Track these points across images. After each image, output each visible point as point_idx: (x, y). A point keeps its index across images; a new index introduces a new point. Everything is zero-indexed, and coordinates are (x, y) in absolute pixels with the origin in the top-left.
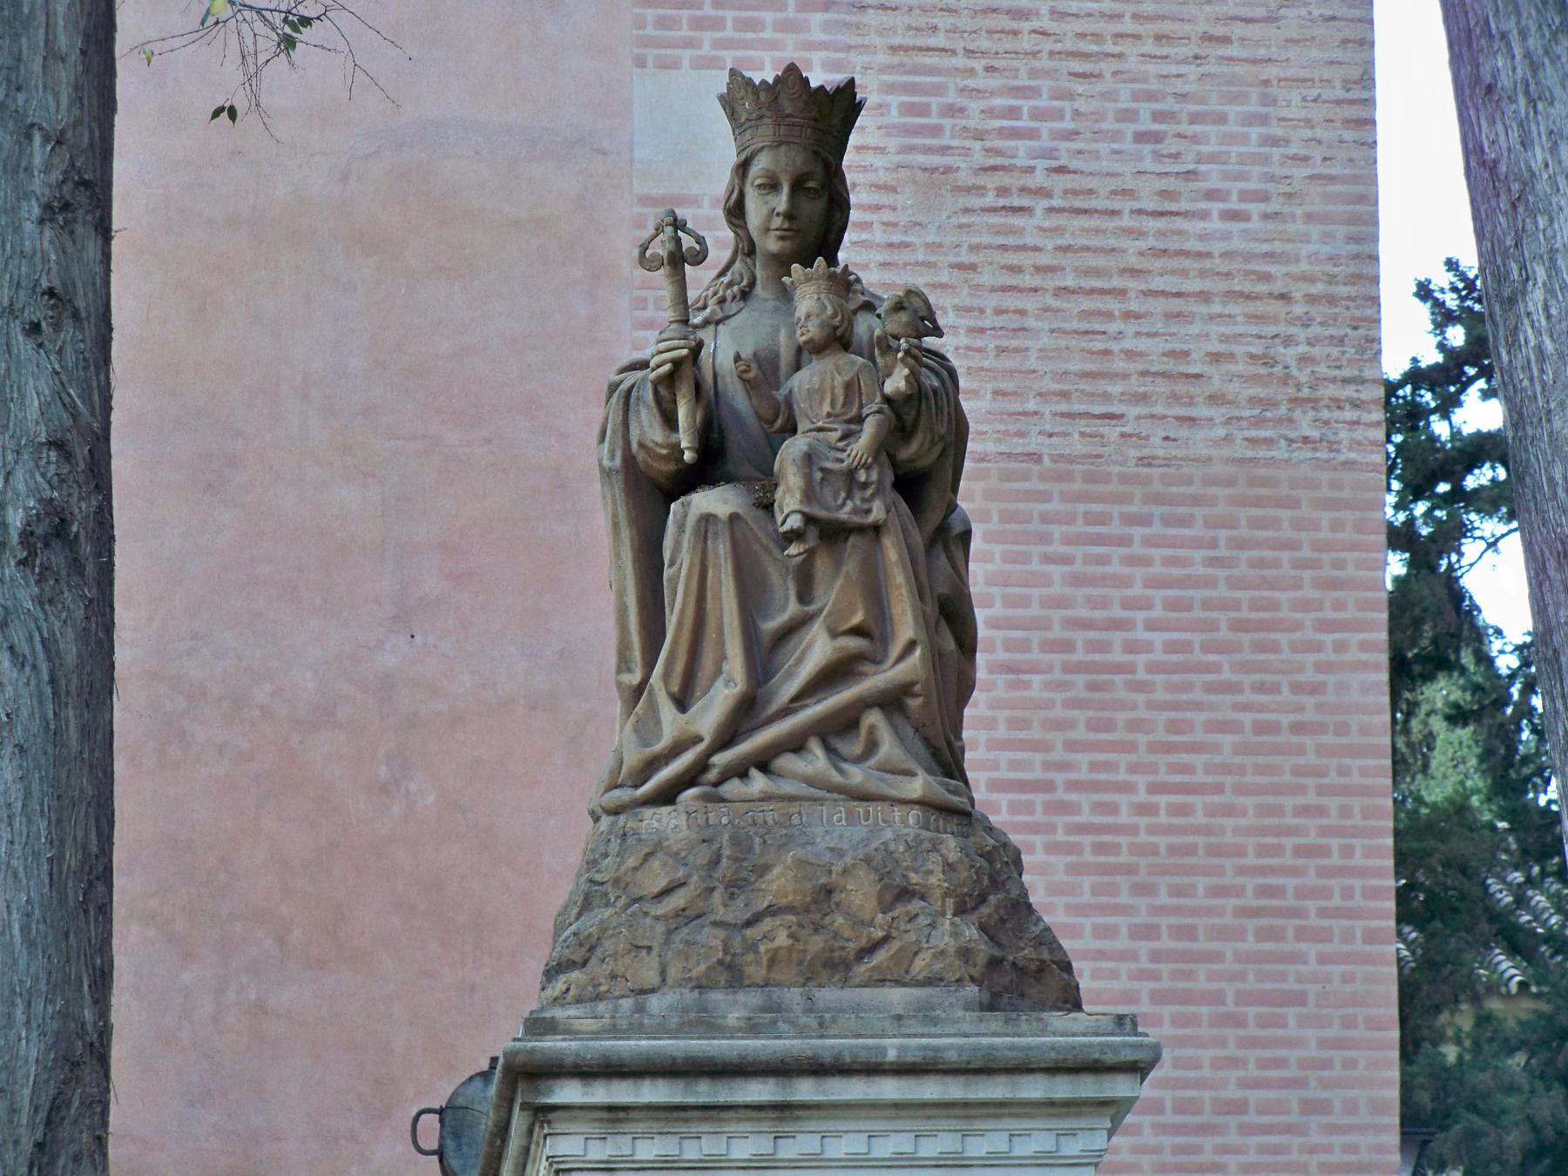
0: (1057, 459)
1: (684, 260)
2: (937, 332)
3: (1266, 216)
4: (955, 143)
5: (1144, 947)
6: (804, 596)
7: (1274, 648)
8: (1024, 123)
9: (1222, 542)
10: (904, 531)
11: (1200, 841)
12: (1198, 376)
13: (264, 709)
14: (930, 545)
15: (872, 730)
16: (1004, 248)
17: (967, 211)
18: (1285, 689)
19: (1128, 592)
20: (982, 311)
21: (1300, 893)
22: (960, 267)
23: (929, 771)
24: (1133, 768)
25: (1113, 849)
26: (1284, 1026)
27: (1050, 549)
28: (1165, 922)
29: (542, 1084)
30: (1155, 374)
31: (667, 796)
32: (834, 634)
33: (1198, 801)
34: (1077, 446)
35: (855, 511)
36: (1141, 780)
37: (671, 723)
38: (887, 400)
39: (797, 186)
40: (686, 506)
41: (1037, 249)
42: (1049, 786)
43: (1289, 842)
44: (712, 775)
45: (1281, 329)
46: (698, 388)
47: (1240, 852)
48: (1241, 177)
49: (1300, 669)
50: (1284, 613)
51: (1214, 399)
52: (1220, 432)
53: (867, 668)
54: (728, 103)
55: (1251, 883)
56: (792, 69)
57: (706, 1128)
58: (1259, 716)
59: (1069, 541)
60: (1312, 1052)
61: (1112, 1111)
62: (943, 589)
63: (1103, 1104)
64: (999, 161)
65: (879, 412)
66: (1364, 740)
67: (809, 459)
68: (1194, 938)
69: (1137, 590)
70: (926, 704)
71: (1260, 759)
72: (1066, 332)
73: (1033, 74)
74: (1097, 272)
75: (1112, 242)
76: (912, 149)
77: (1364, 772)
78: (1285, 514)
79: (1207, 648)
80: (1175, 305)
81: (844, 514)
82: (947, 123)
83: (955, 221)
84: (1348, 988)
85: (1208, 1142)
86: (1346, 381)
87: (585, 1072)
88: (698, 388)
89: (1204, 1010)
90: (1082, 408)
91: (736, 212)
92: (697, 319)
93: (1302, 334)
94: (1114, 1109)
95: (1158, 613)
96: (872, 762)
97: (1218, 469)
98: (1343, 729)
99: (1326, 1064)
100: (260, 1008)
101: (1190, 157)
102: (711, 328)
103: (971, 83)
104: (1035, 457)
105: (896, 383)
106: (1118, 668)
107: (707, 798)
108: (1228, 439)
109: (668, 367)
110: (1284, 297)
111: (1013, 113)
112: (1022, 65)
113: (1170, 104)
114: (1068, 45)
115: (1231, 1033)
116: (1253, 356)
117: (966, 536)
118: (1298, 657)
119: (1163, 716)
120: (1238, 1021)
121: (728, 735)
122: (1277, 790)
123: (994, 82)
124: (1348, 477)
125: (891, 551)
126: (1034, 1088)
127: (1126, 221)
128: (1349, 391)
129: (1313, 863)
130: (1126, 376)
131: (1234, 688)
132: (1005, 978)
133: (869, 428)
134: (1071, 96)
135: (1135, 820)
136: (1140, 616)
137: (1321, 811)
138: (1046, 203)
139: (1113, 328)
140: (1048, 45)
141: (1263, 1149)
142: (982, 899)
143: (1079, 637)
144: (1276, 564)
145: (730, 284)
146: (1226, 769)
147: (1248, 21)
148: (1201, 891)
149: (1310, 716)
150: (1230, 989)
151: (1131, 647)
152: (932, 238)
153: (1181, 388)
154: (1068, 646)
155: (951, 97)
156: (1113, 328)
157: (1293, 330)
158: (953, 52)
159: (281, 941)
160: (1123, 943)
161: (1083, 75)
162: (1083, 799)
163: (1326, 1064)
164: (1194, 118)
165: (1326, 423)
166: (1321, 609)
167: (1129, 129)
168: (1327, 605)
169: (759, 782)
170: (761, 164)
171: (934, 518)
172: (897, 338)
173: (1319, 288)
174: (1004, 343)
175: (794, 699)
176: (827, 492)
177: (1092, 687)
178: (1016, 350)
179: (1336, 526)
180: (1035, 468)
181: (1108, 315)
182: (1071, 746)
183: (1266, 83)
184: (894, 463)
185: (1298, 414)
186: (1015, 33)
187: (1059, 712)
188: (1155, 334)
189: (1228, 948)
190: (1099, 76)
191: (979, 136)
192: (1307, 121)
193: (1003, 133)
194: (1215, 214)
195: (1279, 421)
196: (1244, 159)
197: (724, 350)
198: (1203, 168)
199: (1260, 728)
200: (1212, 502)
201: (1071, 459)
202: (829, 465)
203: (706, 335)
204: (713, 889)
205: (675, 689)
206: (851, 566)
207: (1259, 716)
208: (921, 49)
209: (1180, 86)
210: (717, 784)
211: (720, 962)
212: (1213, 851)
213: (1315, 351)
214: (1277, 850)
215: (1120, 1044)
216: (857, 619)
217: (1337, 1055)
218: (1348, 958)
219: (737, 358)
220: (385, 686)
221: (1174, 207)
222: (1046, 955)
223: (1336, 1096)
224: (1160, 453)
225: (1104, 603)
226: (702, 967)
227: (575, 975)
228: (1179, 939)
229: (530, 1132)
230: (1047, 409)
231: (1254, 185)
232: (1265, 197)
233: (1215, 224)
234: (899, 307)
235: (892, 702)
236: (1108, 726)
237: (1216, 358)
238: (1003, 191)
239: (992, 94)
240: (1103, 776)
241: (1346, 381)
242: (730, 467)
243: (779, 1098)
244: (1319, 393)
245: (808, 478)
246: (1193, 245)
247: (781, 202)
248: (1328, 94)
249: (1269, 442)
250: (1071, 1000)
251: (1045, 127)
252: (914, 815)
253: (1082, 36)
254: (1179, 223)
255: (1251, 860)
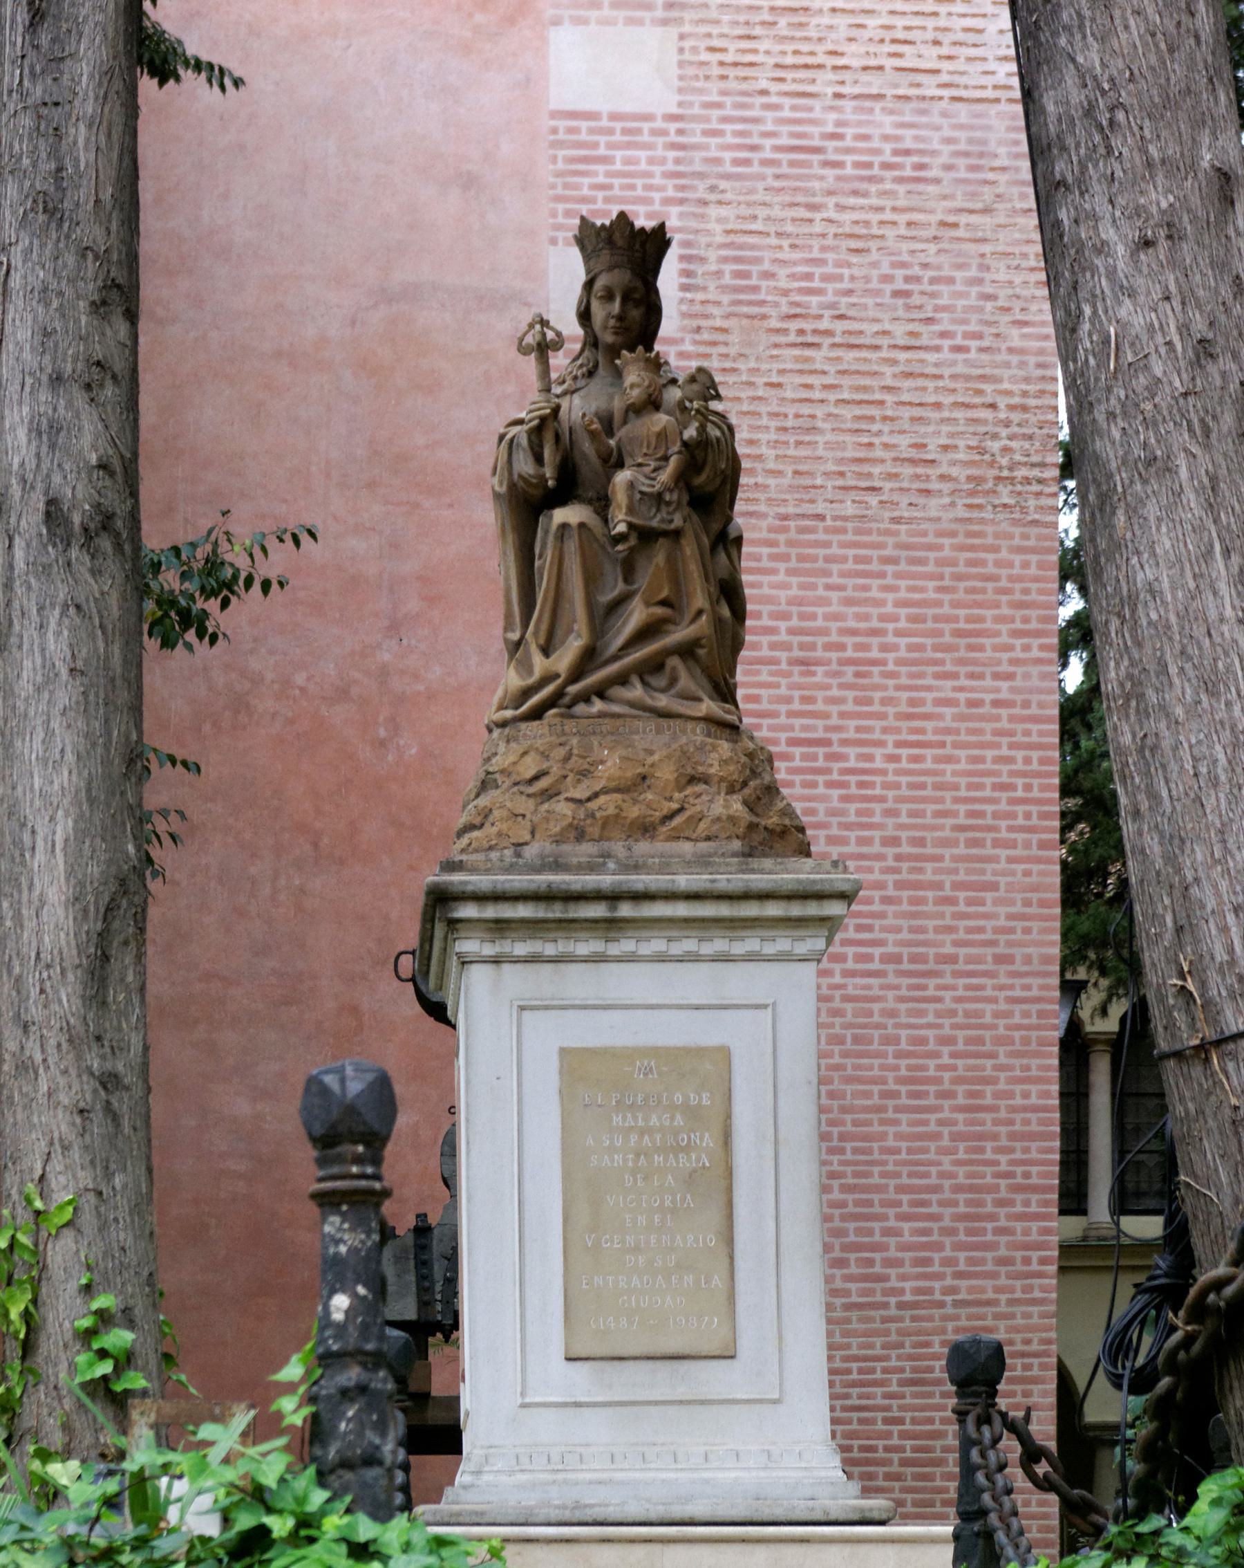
0: (835, 518)
1: (548, 347)
2: (718, 397)
3: (981, 350)
4: (769, 298)
5: (890, 851)
6: (627, 580)
7: (981, 648)
8: (816, 284)
9: (947, 576)
10: (697, 537)
11: (929, 780)
12: (933, 461)
13: (302, 689)
14: (713, 549)
15: (674, 669)
16: (801, 372)
17: (776, 346)
18: (988, 676)
19: (883, 610)
20: (786, 416)
21: (996, 815)
22: (772, 385)
23: (712, 698)
24: (885, 730)
25: (871, 785)
26: (984, 904)
27: (830, 581)
28: (904, 835)
29: (453, 904)
30: (904, 460)
31: (536, 714)
32: (648, 604)
33: (929, 753)
34: (849, 509)
35: (662, 521)
36: (890, 739)
37: (540, 664)
38: (685, 444)
39: (625, 299)
40: (551, 517)
41: (824, 373)
42: (827, 743)
43: (988, 781)
44: (566, 700)
45: (989, 428)
46: (557, 437)
47: (956, 787)
48: (964, 322)
49: (999, 663)
50: (988, 625)
51: (943, 478)
52: (947, 500)
53: (671, 627)
54: (581, 241)
55: (962, 808)
56: (622, 216)
57: (560, 934)
58: (969, 695)
59: (842, 574)
60: (1002, 922)
61: (829, 924)
62: (723, 573)
63: (823, 920)
64: (798, 311)
65: (679, 452)
66: (1041, 712)
67: (631, 485)
68: (924, 846)
69: (889, 609)
70: (709, 653)
71: (971, 725)
72: (843, 431)
73: (823, 249)
74: (865, 389)
75: (875, 368)
76: (740, 302)
77: (1041, 733)
78: (990, 557)
79: (937, 648)
80: (917, 412)
81: (655, 523)
82: (764, 284)
83: (768, 353)
84: (1027, 879)
85: (932, 982)
86: (1033, 465)
87: (481, 898)
88: (557, 437)
89: (930, 894)
90: (853, 483)
91: (585, 316)
92: (557, 390)
93: (1004, 432)
94: (829, 924)
95: (902, 624)
96: (673, 692)
97: (945, 525)
98: (1026, 704)
99: (1011, 931)
100: (302, 890)
101: (930, 308)
102: (568, 397)
103: (780, 256)
104: (821, 517)
105: (690, 432)
106: (874, 662)
107: (562, 715)
108: (953, 504)
109: (536, 422)
110: (993, 406)
111: (808, 277)
112: (816, 243)
113: (916, 271)
114: (847, 230)
115: (949, 910)
116: (970, 448)
117: (739, 541)
118: (997, 655)
119: (904, 695)
120: (952, 901)
121: (577, 674)
122: (982, 745)
123: (797, 255)
124: (1034, 531)
125: (689, 548)
126: (773, 909)
127: (884, 354)
128: (1036, 473)
129: (1004, 795)
130: (883, 461)
131: (954, 676)
132: (757, 838)
133: (673, 461)
134: (849, 265)
135: (885, 765)
136: (891, 626)
137: (1011, 760)
138: (830, 341)
139: (875, 427)
140: (832, 230)
141: (968, 988)
142: (745, 784)
143: (849, 641)
144: (983, 591)
145: (581, 366)
146: (948, 731)
147: (971, 212)
148: (929, 814)
149: (1004, 695)
150: (948, 880)
151: (884, 648)
152: (752, 365)
153: (920, 470)
154: (841, 647)
155: (766, 266)
156: (875, 427)
157: (998, 429)
158: (768, 234)
159: (316, 845)
160: (876, 848)
161: (857, 251)
162: (852, 751)
163: (1011, 931)
164: (933, 281)
165: (1019, 493)
166: (1013, 622)
167: (888, 288)
168: (1018, 619)
169: (598, 705)
170: (600, 283)
171: (716, 527)
172: (691, 401)
173: (1016, 400)
174: (801, 438)
175: (621, 649)
176: (644, 508)
177: (858, 675)
178: (809, 443)
179: (1025, 565)
180: (821, 524)
181: (872, 419)
182: (843, 715)
183: (983, 255)
184: (689, 488)
185: (1000, 488)
186: (811, 221)
187: (835, 692)
188: (904, 432)
189: (947, 853)
190: (868, 251)
191: (786, 293)
192: (1010, 282)
193: (801, 291)
194: (946, 349)
195: (988, 493)
196: (967, 309)
197: (576, 409)
198: (938, 316)
199: (972, 703)
200: (940, 548)
201: (845, 519)
202: (645, 489)
203: (565, 403)
204: (565, 777)
205: (542, 641)
206: (660, 558)
207: (969, 695)
208: (745, 232)
209: (923, 258)
210: (569, 707)
211: (570, 825)
212: (938, 787)
213: (1014, 444)
214: (981, 787)
215: (838, 880)
216: (664, 593)
217: (1019, 925)
218: (1029, 860)
219: (584, 415)
220: (384, 672)
221: (918, 343)
222: (787, 822)
223: (1018, 952)
224: (906, 514)
225: (867, 618)
226: (558, 829)
227: (476, 834)
228: (915, 846)
229: (446, 938)
230: (829, 484)
231: (972, 328)
232: (980, 336)
233: (946, 355)
234: (692, 379)
235: (687, 651)
236: (869, 702)
237: (945, 448)
238: (801, 332)
239: (795, 263)
240: (864, 736)
241: (1033, 465)
242: (580, 492)
243: (608, 915)
244: (1015, 474)
245: (630, 498)
246: (930, 370)
247: (616, 306)
248: (1024, 264)
249: (980, 507)
250: (804, 851)
251: (830, 287)
252: (700, 728)
253: (857, 222)
254: (921, 355)
255: (963, 793)
